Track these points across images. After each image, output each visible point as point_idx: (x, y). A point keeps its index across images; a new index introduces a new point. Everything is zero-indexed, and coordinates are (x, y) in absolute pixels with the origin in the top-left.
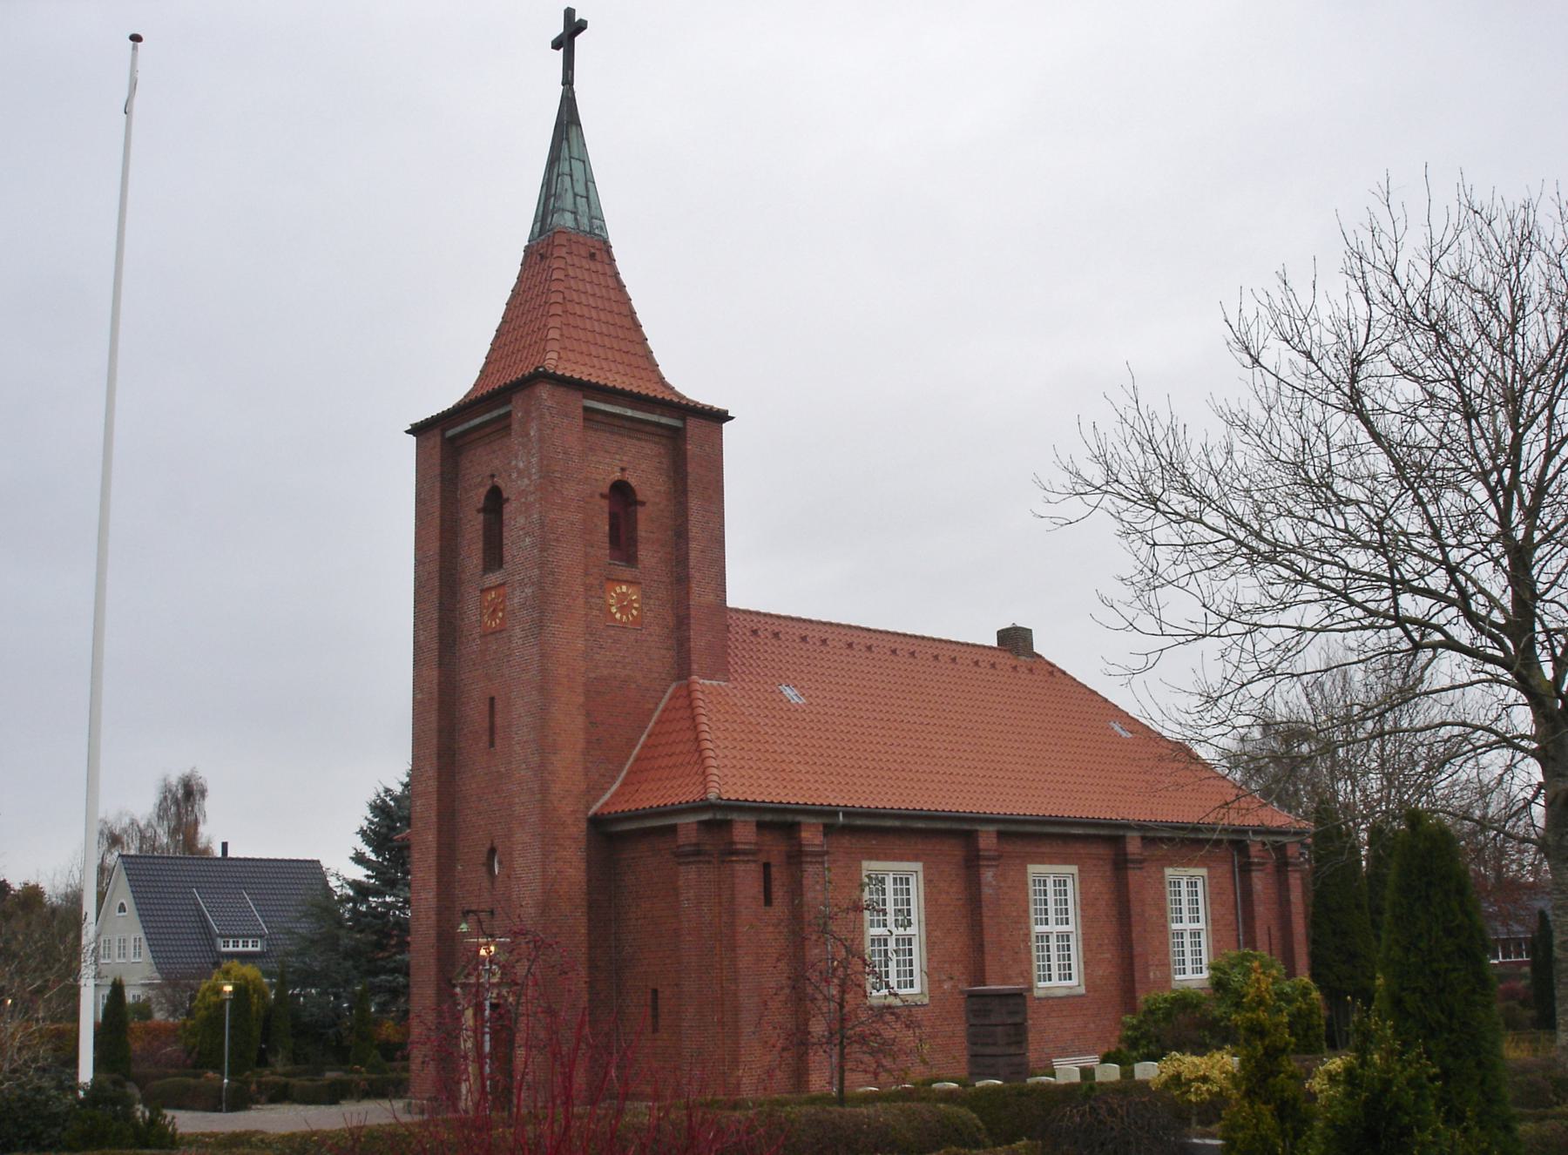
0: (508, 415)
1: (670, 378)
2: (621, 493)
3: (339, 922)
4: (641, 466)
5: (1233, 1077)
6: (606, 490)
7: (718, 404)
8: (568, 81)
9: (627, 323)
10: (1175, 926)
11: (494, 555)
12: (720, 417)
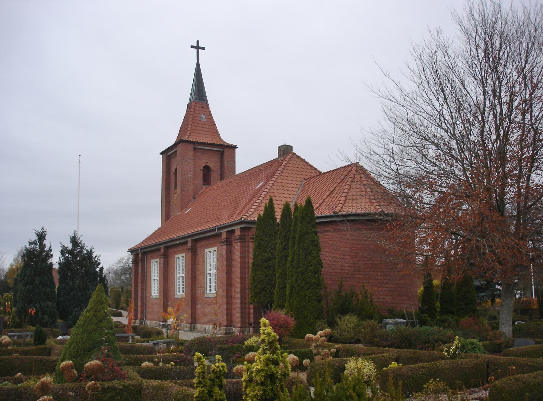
0: (176, 151)
1: (225, 140)
2: (207, 169)
3: (410, 262)
4: (213, 163)
5: (49, 338)
6: (202, 168)
7: (234, 144)
8: (198, 60)
9: (212, 124)
10: (215, 271)
11: (176, 188)
12: (235, 147)
